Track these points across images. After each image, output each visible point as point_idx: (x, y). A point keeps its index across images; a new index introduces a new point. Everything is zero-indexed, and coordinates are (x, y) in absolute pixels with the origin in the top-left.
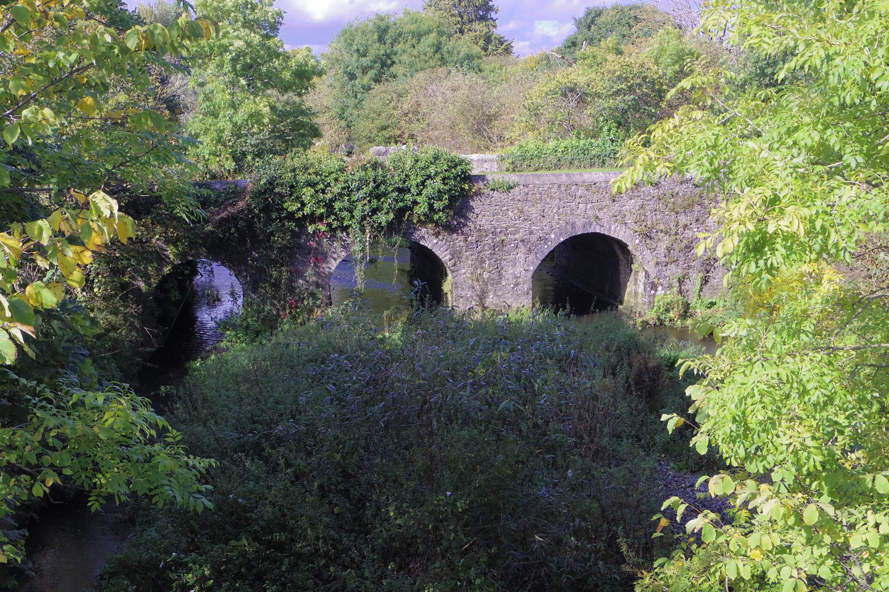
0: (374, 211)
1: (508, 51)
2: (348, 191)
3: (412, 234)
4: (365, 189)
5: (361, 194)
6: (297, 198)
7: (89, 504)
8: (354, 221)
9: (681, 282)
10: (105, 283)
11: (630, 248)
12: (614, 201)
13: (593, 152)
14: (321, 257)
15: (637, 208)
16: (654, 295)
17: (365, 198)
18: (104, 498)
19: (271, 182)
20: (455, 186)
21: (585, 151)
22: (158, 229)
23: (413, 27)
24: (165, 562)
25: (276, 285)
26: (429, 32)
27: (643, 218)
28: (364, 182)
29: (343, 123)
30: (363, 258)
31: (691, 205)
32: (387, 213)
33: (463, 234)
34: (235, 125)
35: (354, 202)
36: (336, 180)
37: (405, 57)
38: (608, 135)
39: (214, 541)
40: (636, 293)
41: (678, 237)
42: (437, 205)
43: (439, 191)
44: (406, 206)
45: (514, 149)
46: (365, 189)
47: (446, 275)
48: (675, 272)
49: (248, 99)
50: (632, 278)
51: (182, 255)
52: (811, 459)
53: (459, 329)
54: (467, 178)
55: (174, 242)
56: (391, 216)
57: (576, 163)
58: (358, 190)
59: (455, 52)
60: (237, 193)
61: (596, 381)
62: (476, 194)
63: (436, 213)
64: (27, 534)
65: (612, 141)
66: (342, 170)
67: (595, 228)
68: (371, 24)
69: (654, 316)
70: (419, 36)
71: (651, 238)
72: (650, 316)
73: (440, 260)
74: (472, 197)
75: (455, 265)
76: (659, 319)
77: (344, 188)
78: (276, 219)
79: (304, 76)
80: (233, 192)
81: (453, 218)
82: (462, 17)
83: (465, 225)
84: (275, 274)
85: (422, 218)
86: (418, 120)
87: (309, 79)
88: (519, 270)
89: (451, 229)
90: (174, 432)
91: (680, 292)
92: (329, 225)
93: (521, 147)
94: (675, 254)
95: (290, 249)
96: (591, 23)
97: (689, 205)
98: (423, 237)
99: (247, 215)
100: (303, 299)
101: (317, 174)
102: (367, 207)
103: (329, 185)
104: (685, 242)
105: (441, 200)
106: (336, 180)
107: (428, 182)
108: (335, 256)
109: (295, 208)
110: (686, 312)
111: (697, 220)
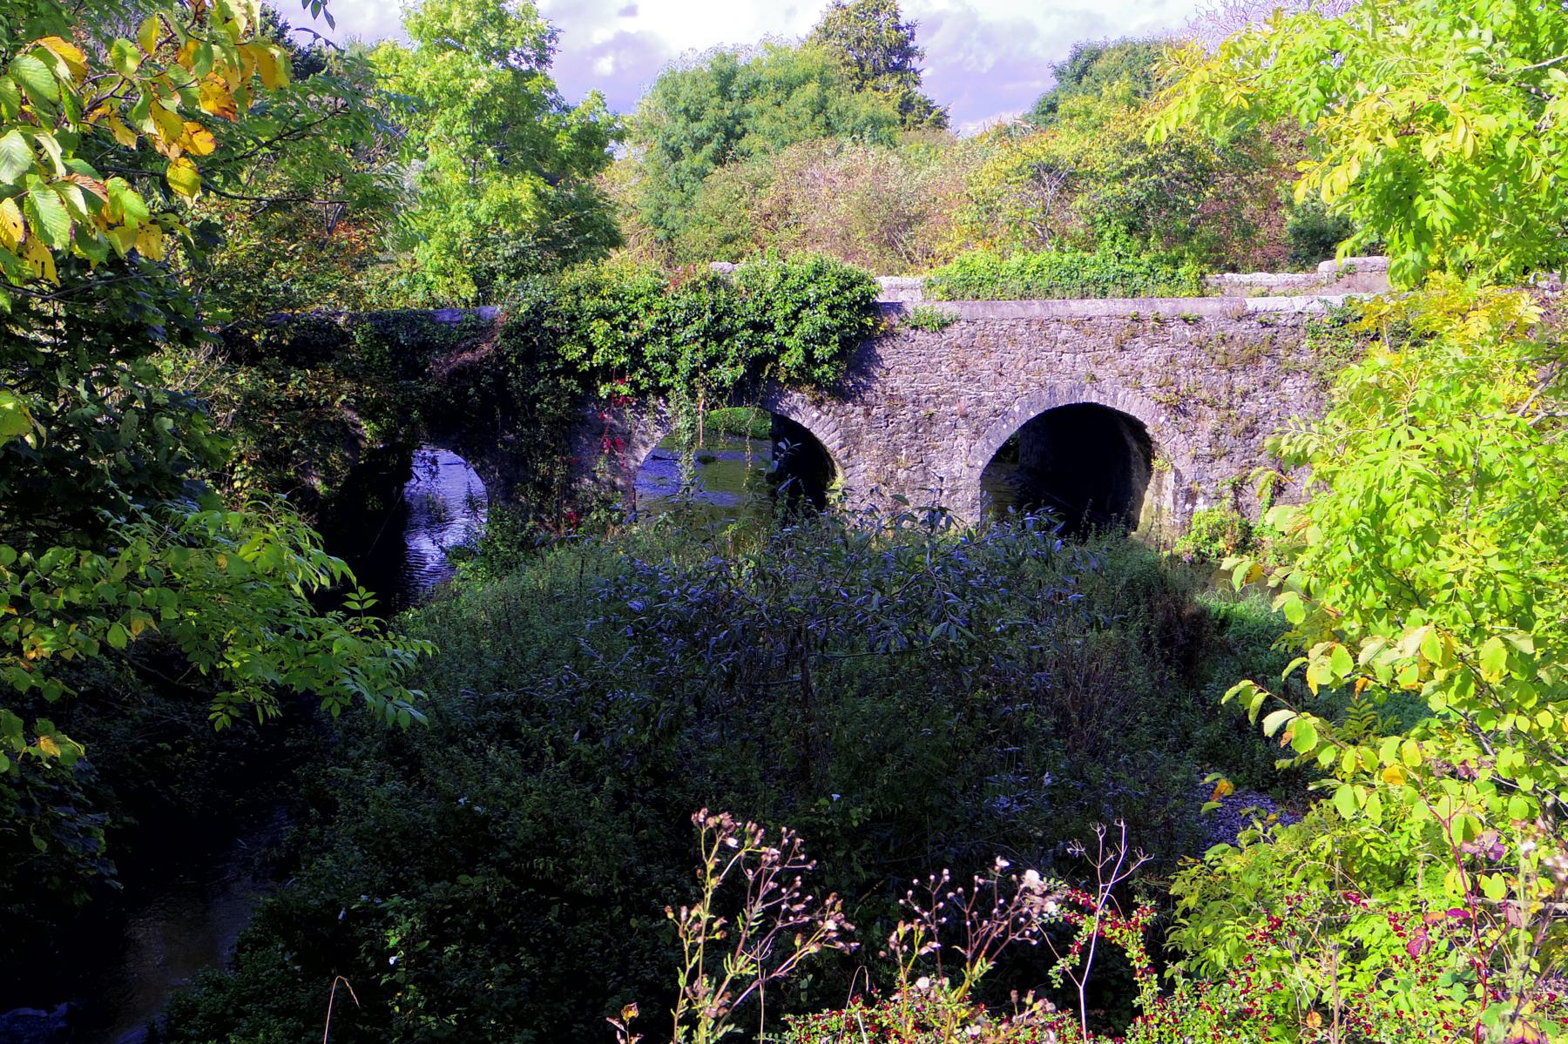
0: (712, 362)
1: (940, 123)
2: (667, 327)
3: (776, 402)
4: (697, 324)
5: (689, 332)
6: (582, 337)
7: (212, 717)
8: (678, 377)
9: (1237, 490)
10: (252, 473)
11: (1150, 431)
12: (1122, 349)
13: (1087, 275)
14: (623, 441)
15: (1162, 361)
16: (1191, 512)
17: (696, 339)
18: (238, 706)
19: (538, 310)
20: (850, 320)
21: (1071, 273)
22: (346, 385)
23: (780, 73)
24: (348, 910)
25: (544, 487)
26: (807, 78)
27: (1172, 378)
28: (695, 311)
29: (661, 234)
30: (691, 442)
31: (1254, 359)
32: (734, 365)
33: (863, 402)
34: (477, 224)
35: (677, 345)
36: (648, 308)
37: (764, 122)
38: (1112, 247)
39: (431, 877)
40: (1159, 508)
41: (1232, 412)
42: (819, 352)
43: (823, 329)
44: (766, 353)
45: (952, 268)
46: (697, 324)
47: (834, 474)
48: (1225, 472)
49: (500, 180)
50: (1152, 484)
51: (388, 435)
52: (1503, 593)
53: (854, 552)
54: (869, 306)
55: (371, 411)
56: (741, 369)
57: (1057, 292)
58: (685, 324)
59: (850, 114)
60: (482, 330)
61: (1093, 643)
62: (886, 334)
63: (818, 366)
64: (108, 821)
65: (1120, 257)
66: (659, 291)
67: (1089, 395)
68: (706, 68)
69: (1190, 546)
70: (788, 87)
71: (1185, 414)
72: (1184, 546)
73: (823, 448)
74: (879, 339)
75: (848, 456)
76: (1198, 551)
77: (660, 322)
78: (546, 373)
79: (592, 144)
80: (473, 328)
81: (846, 376)
82: (862, 67)
83: (867, 388)
84: (543, 468)
85: (794, 374)
86: (787, 226)
87: (603, 145)
88: (958, 466)
89: (841, 394)
90: (362, 590)
91: (1237, 507)
92: (635, 384)
93: (963, 264)
94: (1227, 440)
95: (569, 424)
96: (1082, 68)
97: (1252, 358)
98: (796, 408)
99: (496, 366)
100: (590, 510)
101: (615, 297)
102: (700, 355)
103: (635, 316)
104: (1245, 421)
105: (827, 344)
106: (648, 308)
107: (804, 313)
108: (646, 438)
109: (576, 355)
110: (1245, 541)
111: (1266, 384)
